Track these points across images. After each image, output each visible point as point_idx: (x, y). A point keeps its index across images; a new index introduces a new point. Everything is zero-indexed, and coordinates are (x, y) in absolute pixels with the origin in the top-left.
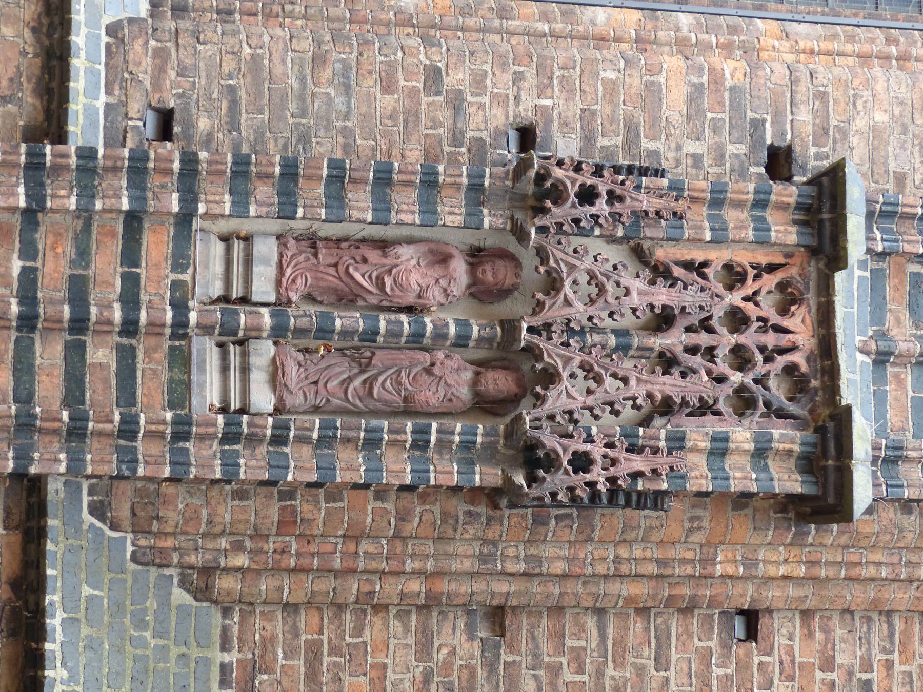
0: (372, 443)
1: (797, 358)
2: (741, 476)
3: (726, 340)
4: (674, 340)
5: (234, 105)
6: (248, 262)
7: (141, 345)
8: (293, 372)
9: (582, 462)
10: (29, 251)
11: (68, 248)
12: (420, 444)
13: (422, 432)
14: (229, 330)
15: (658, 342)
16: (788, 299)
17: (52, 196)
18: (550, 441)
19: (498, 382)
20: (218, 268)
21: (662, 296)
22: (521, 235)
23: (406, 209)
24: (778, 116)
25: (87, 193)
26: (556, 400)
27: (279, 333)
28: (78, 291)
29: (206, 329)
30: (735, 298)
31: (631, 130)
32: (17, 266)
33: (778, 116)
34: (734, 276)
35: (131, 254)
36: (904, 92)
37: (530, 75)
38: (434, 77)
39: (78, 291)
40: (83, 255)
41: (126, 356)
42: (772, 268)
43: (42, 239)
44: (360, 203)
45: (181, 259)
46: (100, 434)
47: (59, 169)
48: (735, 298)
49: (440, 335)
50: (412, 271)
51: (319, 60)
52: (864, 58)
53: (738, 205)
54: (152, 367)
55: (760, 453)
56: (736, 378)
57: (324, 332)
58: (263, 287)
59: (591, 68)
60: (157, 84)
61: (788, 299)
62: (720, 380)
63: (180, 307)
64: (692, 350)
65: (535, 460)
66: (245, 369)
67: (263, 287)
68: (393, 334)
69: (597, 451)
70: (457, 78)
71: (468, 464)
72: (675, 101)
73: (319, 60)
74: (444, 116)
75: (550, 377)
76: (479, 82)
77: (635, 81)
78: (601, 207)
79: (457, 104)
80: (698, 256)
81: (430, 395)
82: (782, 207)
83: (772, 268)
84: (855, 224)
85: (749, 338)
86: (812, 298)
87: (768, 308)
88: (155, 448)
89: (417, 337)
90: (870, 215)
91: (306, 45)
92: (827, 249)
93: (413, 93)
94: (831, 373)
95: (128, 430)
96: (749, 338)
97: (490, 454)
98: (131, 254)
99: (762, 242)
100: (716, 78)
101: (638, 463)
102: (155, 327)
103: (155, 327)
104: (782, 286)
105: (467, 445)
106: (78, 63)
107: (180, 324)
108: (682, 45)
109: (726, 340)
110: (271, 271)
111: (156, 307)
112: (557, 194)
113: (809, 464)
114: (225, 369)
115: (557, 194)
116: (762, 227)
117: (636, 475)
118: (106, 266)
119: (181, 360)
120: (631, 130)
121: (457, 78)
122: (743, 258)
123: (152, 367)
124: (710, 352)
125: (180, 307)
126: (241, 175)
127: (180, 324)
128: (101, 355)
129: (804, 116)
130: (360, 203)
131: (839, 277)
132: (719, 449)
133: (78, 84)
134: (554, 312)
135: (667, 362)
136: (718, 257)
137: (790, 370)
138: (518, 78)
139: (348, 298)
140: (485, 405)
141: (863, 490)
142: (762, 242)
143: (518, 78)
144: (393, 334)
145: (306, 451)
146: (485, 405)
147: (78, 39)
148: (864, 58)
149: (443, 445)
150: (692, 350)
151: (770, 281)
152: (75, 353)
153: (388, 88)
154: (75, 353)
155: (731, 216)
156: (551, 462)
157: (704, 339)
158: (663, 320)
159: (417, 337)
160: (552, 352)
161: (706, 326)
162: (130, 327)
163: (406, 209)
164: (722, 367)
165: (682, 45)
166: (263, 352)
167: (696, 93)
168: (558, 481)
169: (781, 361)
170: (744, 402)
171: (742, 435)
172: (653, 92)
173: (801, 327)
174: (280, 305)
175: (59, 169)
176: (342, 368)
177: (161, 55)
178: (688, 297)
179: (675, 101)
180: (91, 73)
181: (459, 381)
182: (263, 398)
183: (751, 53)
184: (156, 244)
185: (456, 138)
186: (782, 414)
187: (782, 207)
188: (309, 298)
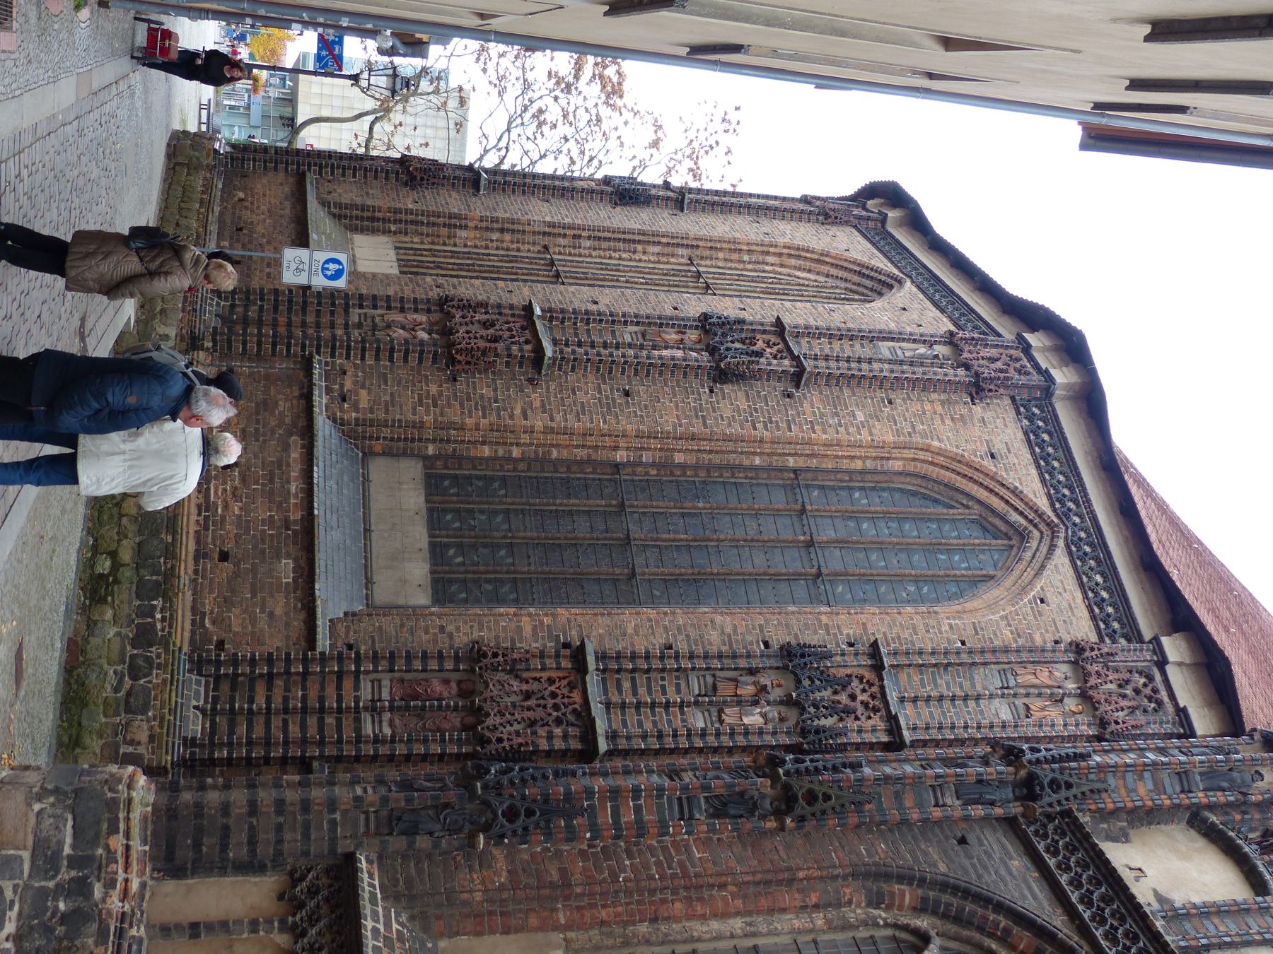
0: (426, 741)
1: (576, 706)
2: (559, 744)
3: (551, 702)
4: (532, 702)
5: (373, 641)
6: (380, 688)
7: (344, 717)
8: (397, 722)
9: (500, 740)
10: (304, 689)
11: (317, 686)
12: (443, 740)
13: (443, 737)
14: (374, 709)
15: (526, 704)
16: (571, 686)
17: (296, 841)
18: (487, 734)
19: (470, 720)
20: (370, 690)
21: (525, 687)
22: (473, 671)
23: (433, 665)
24: (565, 634)
25: (323, 667)
26: (489, 722)
27: (391, 709)
28: (321, 699)
29: (366, 709)
30: (553, 688)
31: (513, 641)
32: (300, 693)
33: (565, 634)
34: (551, 681)
35: (339, 687)
36: (609, 622)
37: (476, 625)
38: (442, 629)
39: (321, 699)
40: (323, 688)
41: (339, 721)
42: (564, 678)
43: (308, 684)
44: (417, 665)
45: (357, 688)
46: (330, 743)
47: (313, 659)
48: (553, 688)
49: (448, 706)
50: (437, 687)
51: (402, 626)
52: (595, 615)
53: (550, 657)
54: (348, 722)
55: (565, 737)
56: (555, 714)
57: (407, 708)
58: (385, 695)
59: (496, 622)
60: (347, 636)
61: (571, 686)
62: (550, 715)
63: (357, 703)
64: (539, 706)
65: (483, 741)
66: (380, 722)
67: (385, 695)
68: (432, 706)
69: (505, 737)
70: (450, 628)
71: (460, 747)
72: (527, 631)
73: (402, 626)
74: (446, 640)
75: (488, 715)
76: (458, 629)
77: (513, 625)
78: (500, 658)
79: (451, 636)
80: (538, 675)
81: (446, 725)
82: (565, 657)
83: (564, 678)
84: (591, 659)
85: (558, 700)
86: (580, 686)
87: (565, 691)
88: (349, 747)
89: (440, 707)
90: (597, 658)
91: (398, 622)
92: (581, 668)
93: (435, 634)
94: (589, 709)
95: (340, 741)
96: (558, 700)
97: (468, 742)
98: (339, 687)
99: (559, 668)
100: (542, 623)
101: (520, 740)
102: (348, 708)
103: (348, 708)
104: (569, 684)
105: (459, 740)
106: (319, 630)
107: (357, 706)
108: (530, 615)
109: (551, 702)
110: (388, 690)
111: (348, 702)
112: (485, 655)
113: (583, 739)
114: (373, 722)
115: (485, 655)
116: (558, 663)
117: (521, 745)
118: (331, 691)
119: (358, 720)
120: (513, 641)
121: (450, 628)
122: (554, 674)
123: (348, 722)
124: (545, 707)
125: (357, 703)
126: (376, 658)
127: (357, 706)
128: (330, 720)
129: (574, 632)
130: (417, 665)
131: (588, 678)
132: (550, 737)
133: (319, 636)
134: (487, 694)
135: (529, 709)
136: (545, 675)
137: (575, 710)
138: (471, 627)
139: (416, 697)
140: (465, 728)
141: (603, 746)
142: (559, 668)
143: (471, 627)
144: (432, 706)
145: (403, 745)
146: (465, 728)
147: (319, 622)
148: (595, 615)
149: (451, 740)
150: (539, 706)
151: (565, 682)
152: (321, 721)
153: (427, 633)
154: (321, 721)
155: (547, 661)
156: (489, 741)
157: (542, 702)
158: (528, 695)
159: (440, 707)
160: (487, 707)
161: (543, 698)
162: (339, 710)
163: (433, 665)
164: (550, 711)
165: (530, 615)
166: (387, 716)
167: (534, 628)
168: (492, 748)
169: (570, 708)
170: (558, 722)
171: (558, 731)
172: (519, 629)
173: (576, 696)
174: (392, 701)
175: (313, 659)
176: (414, 721)
177: (348, 628)
178: (535, 686)
179: (527, 631)
180: (324, 634)
181: (456, 720)
182: (387, 731)
183: (554, 616)
184: (348, 684)
185: (451, 647)
186: (572, 725)
187: (565, 657)
188: (402, 699)
